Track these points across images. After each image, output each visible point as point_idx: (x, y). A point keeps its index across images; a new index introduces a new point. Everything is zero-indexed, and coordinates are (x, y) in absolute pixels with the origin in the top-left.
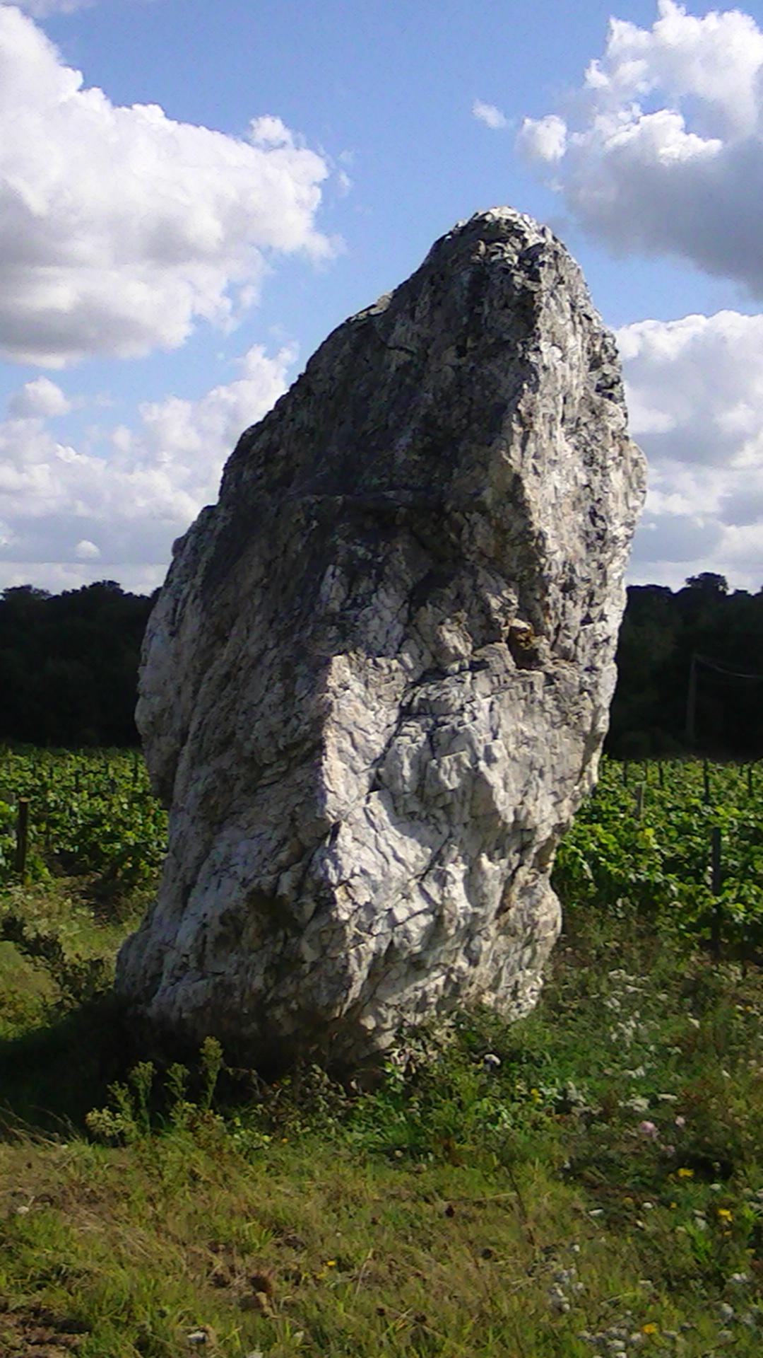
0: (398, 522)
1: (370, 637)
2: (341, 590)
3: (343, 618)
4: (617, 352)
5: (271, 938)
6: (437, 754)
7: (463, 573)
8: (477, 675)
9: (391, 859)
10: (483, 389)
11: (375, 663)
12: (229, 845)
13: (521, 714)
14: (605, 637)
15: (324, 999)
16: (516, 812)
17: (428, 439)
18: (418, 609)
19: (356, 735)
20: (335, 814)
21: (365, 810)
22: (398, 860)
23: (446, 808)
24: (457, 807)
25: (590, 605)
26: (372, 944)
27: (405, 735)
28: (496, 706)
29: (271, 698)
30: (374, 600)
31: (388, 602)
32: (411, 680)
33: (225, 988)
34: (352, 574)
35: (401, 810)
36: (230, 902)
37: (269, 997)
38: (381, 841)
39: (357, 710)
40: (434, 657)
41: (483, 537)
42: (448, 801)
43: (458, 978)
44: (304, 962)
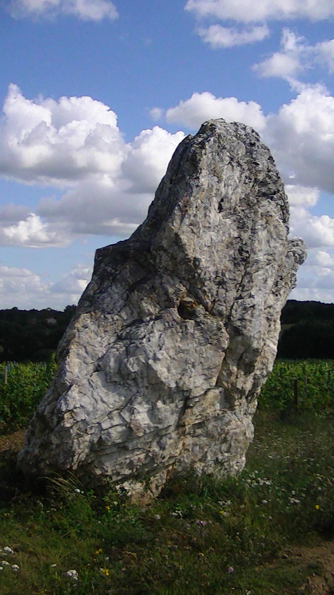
1: (105, 306)
4: (279, 178)
6: (129, 356)
8: (156, 322)
9: (100, 402)
11: (104, 316)
13: (179, 339)
14: (251, 305)
15: (61, 459)
16: (177, 383)
19: (87, 348)
20: (70, 381)
21: (88, 380)
22: (103, 402)
23: (135, 380)
24: (139, 380)
25: (242, 291)
26: (87, 438)
27: (114, 348)
28: (162, 336)
31: (117, 291)
32: (125, 324)
35: (108, 380)
38: (95, 393)
39: (90, 337)
40: (139, 314)
41: (164, 260)
43: (153, 455)
44: (53, 444)
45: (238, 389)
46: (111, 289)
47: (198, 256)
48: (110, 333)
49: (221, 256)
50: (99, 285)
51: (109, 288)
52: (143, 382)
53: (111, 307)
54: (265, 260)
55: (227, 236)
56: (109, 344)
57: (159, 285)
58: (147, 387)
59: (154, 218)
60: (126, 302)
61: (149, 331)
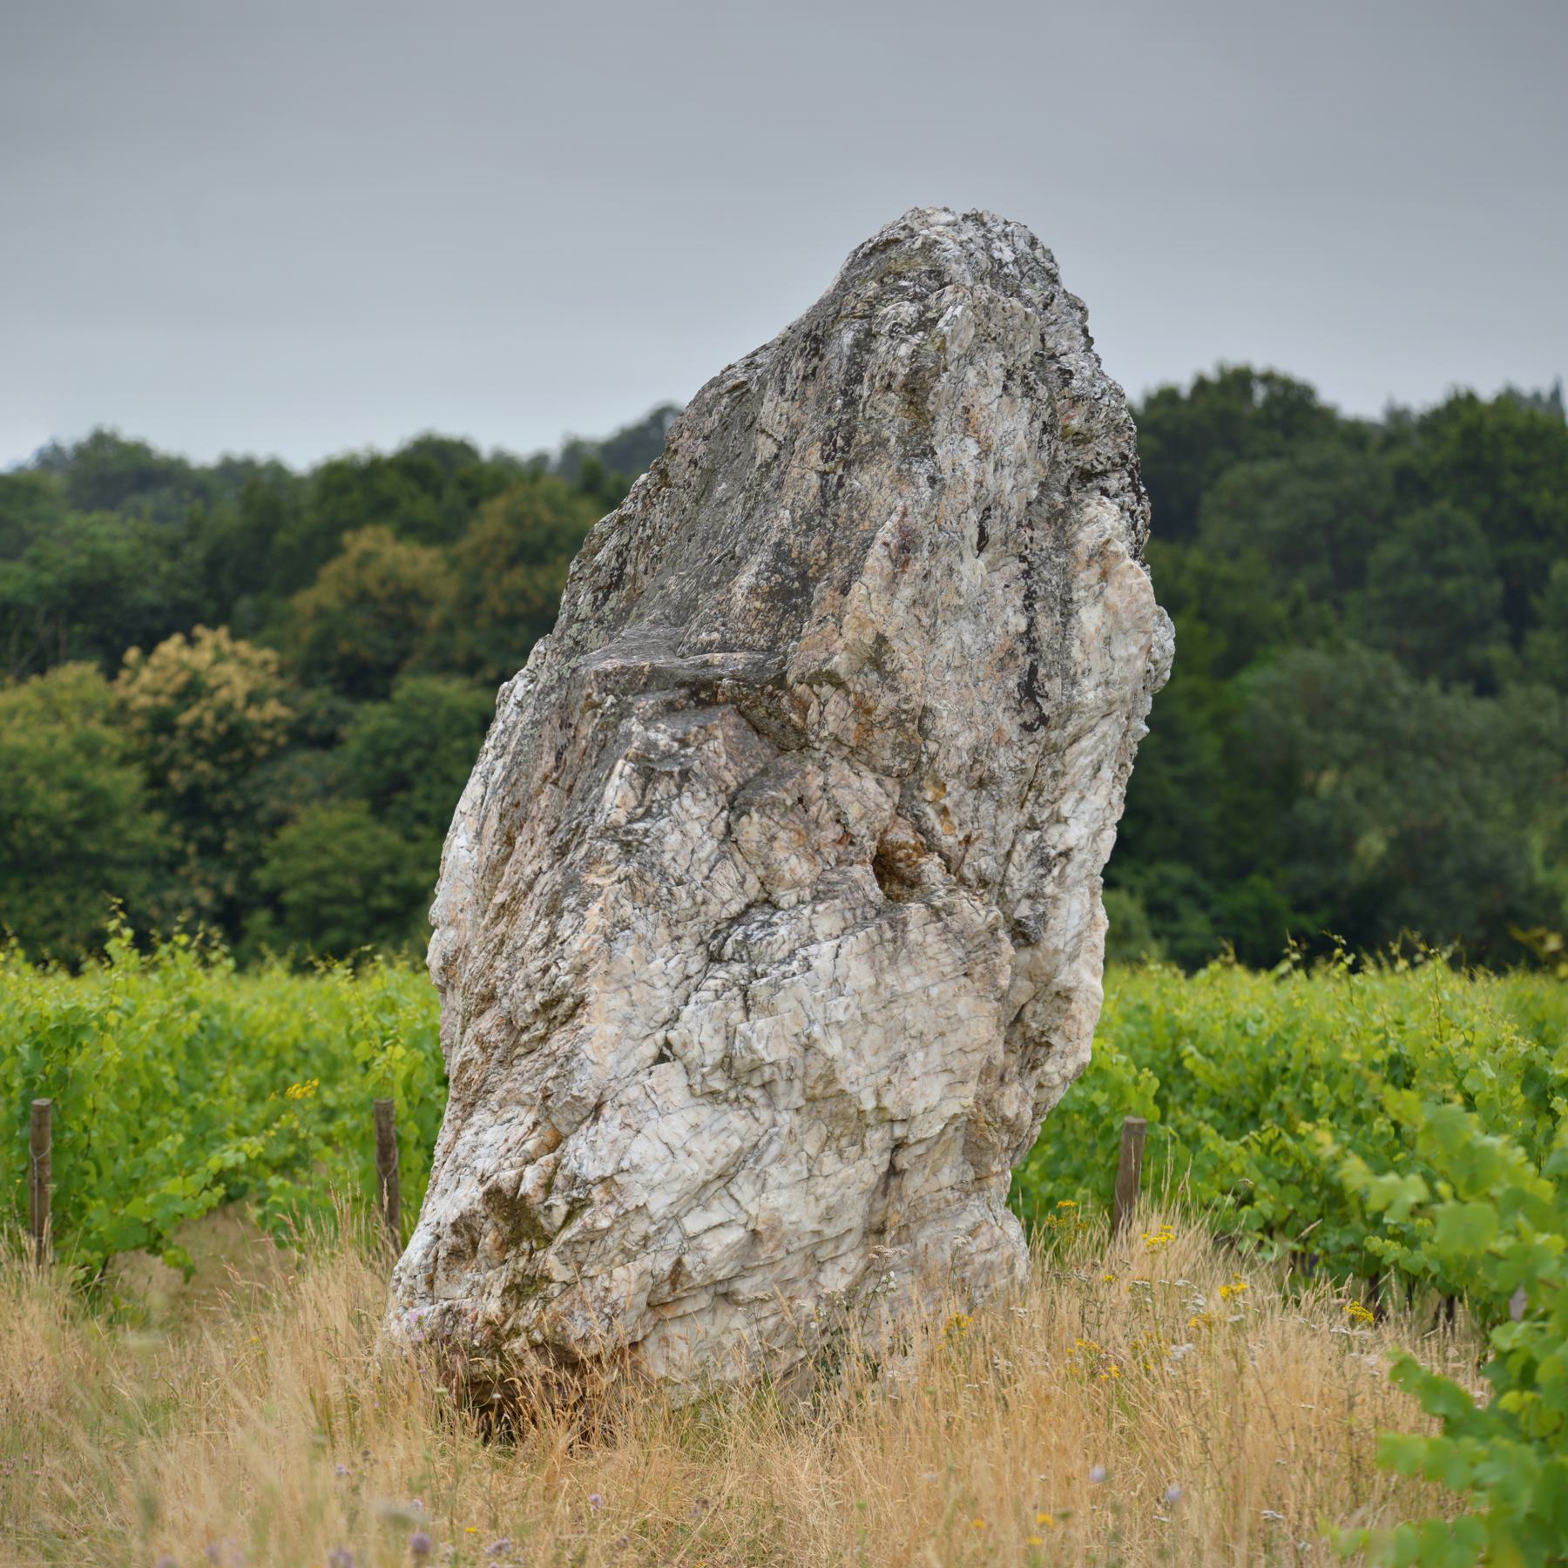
0: (720, 698)
2: (631, 794)
3: (628, 832)
5: (513, 1252)
7: (809, 767)
10: (850, 509)
12: (477, 1134)
14: (1061, 848)
17: (776, 578)
18: (738, 819)
24: (781, 1087)
29: (535, 940)
30: (675, 807)
31: (696, 811)
33: (454, 1314)
34: (647, 773)
36: (464, 1205)
37: (507, 1326)
40: (762, 884)
42: (767, 1078)
45: (1004, 1119)
46: (680, 804)
47: (930, 701)
48: (687, 944)
49: (986, 698)
50: (639, 792)
51: (675, 803)
52: (788, 1094)
53: (683, 862)
54: (1100, 703)
55: (999, 631)
56: (688, 977)
57: (819, 793)
58: (798, 1110)
59: (776, 571)
60: (725, 848)
61: (804, 939)
